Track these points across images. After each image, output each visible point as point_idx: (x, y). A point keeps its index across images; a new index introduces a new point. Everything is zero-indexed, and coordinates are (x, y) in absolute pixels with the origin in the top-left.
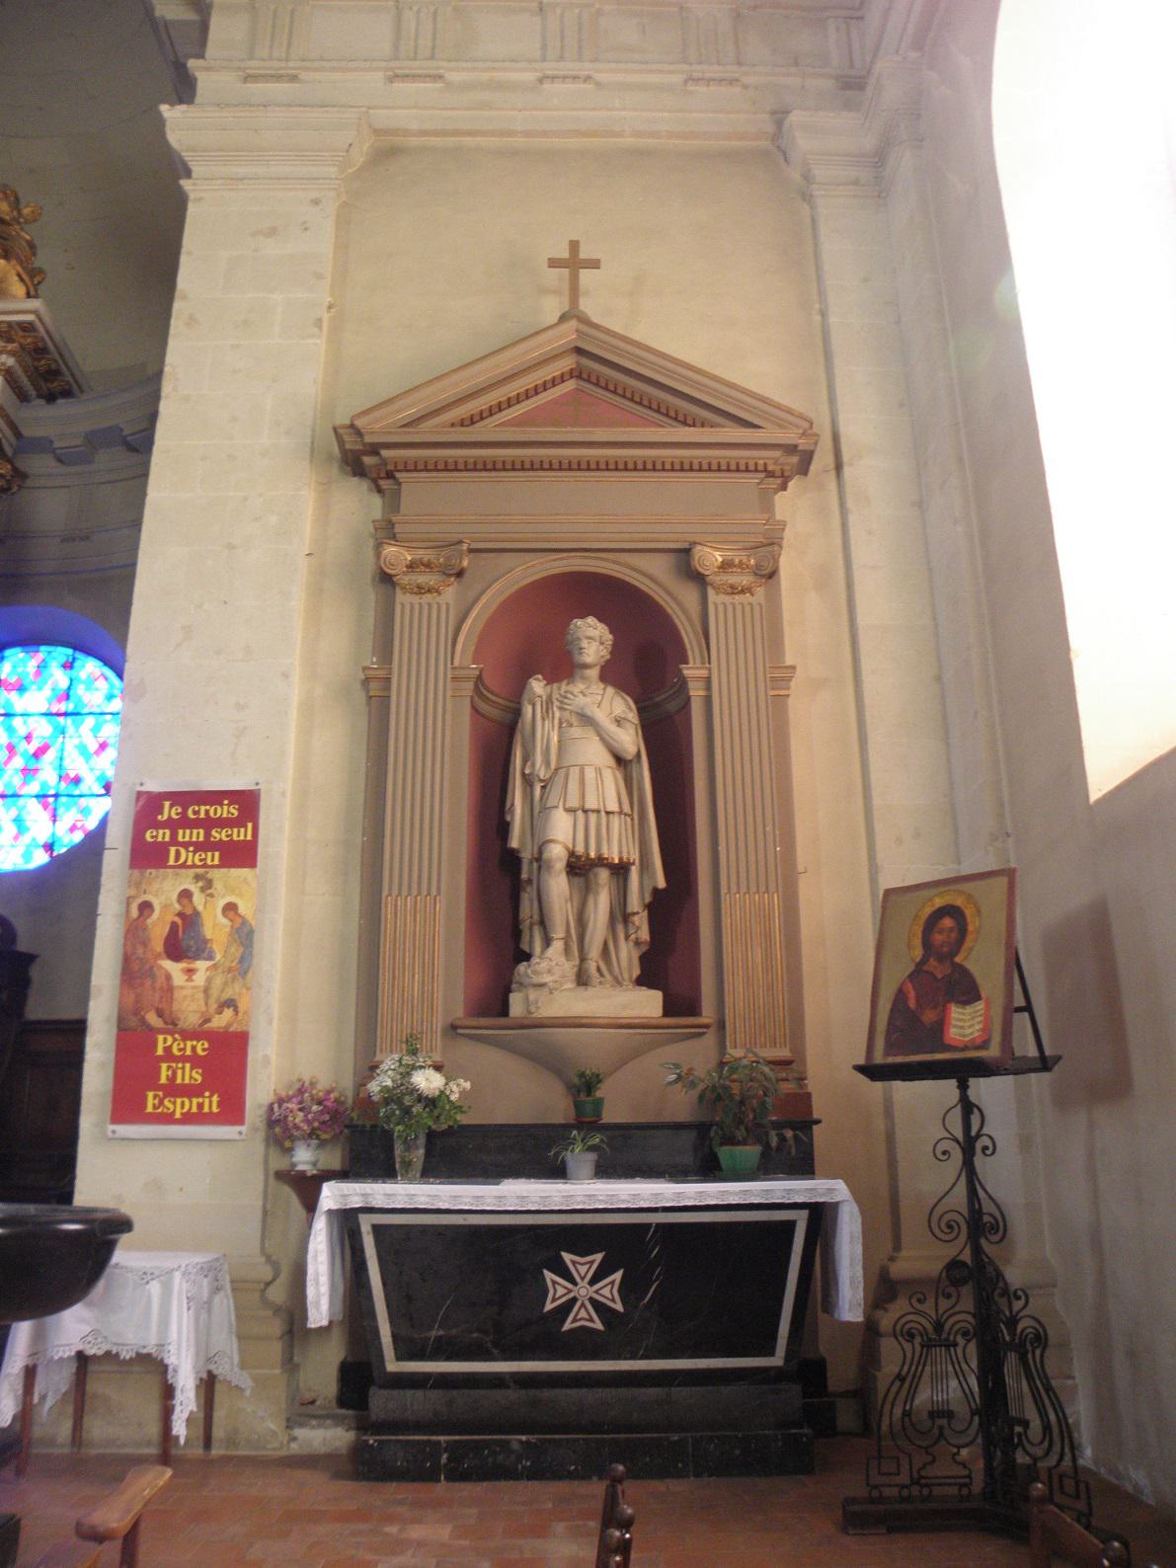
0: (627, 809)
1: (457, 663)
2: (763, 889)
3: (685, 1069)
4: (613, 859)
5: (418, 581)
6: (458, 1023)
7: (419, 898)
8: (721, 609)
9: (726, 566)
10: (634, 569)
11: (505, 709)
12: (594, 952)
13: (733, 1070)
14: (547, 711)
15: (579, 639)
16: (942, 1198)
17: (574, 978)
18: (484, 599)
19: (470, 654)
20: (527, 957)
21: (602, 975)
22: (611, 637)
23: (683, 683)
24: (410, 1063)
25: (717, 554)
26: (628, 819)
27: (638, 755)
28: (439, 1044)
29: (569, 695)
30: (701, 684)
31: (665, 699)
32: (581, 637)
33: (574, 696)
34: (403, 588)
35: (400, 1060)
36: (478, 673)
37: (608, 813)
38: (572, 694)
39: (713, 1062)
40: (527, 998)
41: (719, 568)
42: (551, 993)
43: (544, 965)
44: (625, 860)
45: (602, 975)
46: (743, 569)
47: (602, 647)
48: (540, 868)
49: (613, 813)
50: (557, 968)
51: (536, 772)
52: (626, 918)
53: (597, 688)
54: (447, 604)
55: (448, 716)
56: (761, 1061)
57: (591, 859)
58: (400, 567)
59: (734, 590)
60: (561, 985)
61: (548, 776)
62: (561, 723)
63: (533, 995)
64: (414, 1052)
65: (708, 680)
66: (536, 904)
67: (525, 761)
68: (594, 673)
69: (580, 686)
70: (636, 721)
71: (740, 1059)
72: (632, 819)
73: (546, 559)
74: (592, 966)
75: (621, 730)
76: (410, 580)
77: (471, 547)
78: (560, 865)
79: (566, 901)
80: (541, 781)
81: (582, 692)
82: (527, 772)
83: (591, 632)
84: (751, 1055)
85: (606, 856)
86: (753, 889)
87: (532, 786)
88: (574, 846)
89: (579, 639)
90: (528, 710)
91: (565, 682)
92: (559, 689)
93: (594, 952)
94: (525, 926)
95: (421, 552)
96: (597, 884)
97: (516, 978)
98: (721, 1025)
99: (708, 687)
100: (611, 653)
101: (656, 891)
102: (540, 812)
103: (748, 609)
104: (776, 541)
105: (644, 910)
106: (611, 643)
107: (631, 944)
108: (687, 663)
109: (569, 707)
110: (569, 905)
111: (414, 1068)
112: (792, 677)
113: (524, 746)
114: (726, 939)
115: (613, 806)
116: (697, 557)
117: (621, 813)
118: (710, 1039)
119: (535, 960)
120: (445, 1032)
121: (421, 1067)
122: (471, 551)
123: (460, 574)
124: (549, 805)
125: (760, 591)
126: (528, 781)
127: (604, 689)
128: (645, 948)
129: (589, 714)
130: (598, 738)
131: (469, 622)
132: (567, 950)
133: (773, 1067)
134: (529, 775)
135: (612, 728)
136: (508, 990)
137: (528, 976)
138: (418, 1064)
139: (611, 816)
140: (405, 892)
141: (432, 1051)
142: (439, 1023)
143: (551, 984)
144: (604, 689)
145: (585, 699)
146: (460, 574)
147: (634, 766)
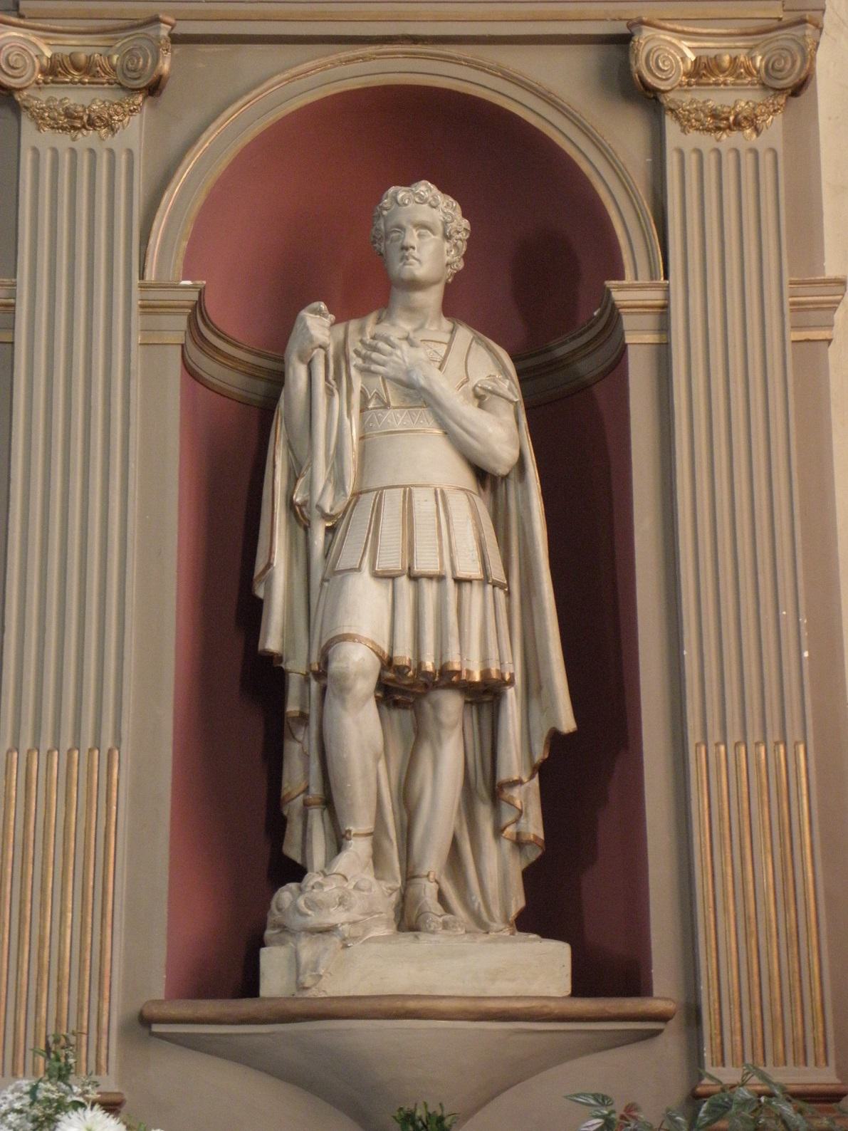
0: (497, 573)
1: (151, 276)
2: (774, 735)
3: (619, 1109)
4: (469, 672)
5: (67, 103)
6: (155, 1011)
7: (76, 754)
8: (692, 160)
9: (702, 71)
10: (507, 77)
11: (252, 372)
12: (432, 861)
13: (720, 1110)
14: (338, 378)
15: (401, 228)
16: (745, 913)
17: (391, 915)
18: (206, 141)
19: (178, 262)
20: (296, 872)
21: (447, 908)
22: (465, 223)
23: (613, 317)
24: (55, 1096)
25: (685, 45)
26: (501, 594)
27: (521, 464)
28: (113, 1054)
29: (382, 345)
30: (650, 321)
31: (574, 352)
32: (404, 223)
33: (393, 346)
34: (38, 119)
35: (33, 1092)
36: (195, 296)
37: (459, 581)
38: (387, 341)
39: (675, 1094)
40: (296, 954)
41: (688, 75)
42: (345, 946)
43: (331, 889)
44: (494, 675)
45: (447, 908)
46: (739, 76)
47: (447, 245)
48: (323, 691)
49: (470, 581)
50: (356, 894)
51: (316, 499)
52: (496, 792)
53: (439, 328)
54: (130, 152)
55: (136, 384)
56: (777, 1092)
57: (426, 674)
58: (29, 70)
59: (721, 122)
60: (366, 930)
61: (338, 509)
62: (365, 400)
63: (307, 950)
64: (62, 1074)
65: (664, 311)
66: (315, 766)
67: (293, 478)
68: (431, 299)
69: (400, 326)
70: (517, 397)
71: (733, 1086)
72: (508, 594)
73: (333, 58)
74: (427, 890)
75: (484, 414)
76: (50, 99)
77: (176, 31)
78: (364, 686)
79: (377, 760)
80: (326, 517)
81: (407, 339)
82: (298, 499)
83: (424, 214)
84: (755, 1079)
85: (456, 667)
86: (754, 735)
87: (307, 529)
88: (392, 647)
89: (401, 228)
90: (298, 374)
91: (372, 318)
92: (362, 330)
93: (432, 861)
94: (293, 809)
95: (73, 40)
96: (439, 723)
97: (274, 916)
98: (693, 1015)
99: (664, 327)
100: (465, 257)
101: (556, 739)
102: (324, 580)
103: (747, 160)
104: (808, 15)
105: (531, 777)
106: (465, 236)
107: (507, 845)
108: (621, 276)
109: (380, 369)
110: (382, 764)
111: (61, 1106)
112: (838, 302)
113: (290, 446)
114: (700, 838)
115: (469, 567)
116: (643, 55)
117: (486, 580)
118: (670, 1044)
119: (312, 878)
120: (125, 1030)
121: (77, 1105)
122: (176, 39)
123: (154, 89)
124: (341, 565)
125: (774, 125)
126: (299, 516)
127: (452, 332)
128: (533, 854)
129: (422, 382)
130: (438, 431)
131: (175, 189)
132: (377, 858)
133: (801, 1105)
134: (304, 504)
135: (467, 410)
136: (257, 942)
137: (297, 910)
138: (69, 1099)
139: (466, 587)
140: (47, 743)
141: (98, 1072)
142: (115, 1011)
143: (346, 927)
144: (452, 332)
145: (413, 351)
146: (154, 89)
147: (513, 489)
